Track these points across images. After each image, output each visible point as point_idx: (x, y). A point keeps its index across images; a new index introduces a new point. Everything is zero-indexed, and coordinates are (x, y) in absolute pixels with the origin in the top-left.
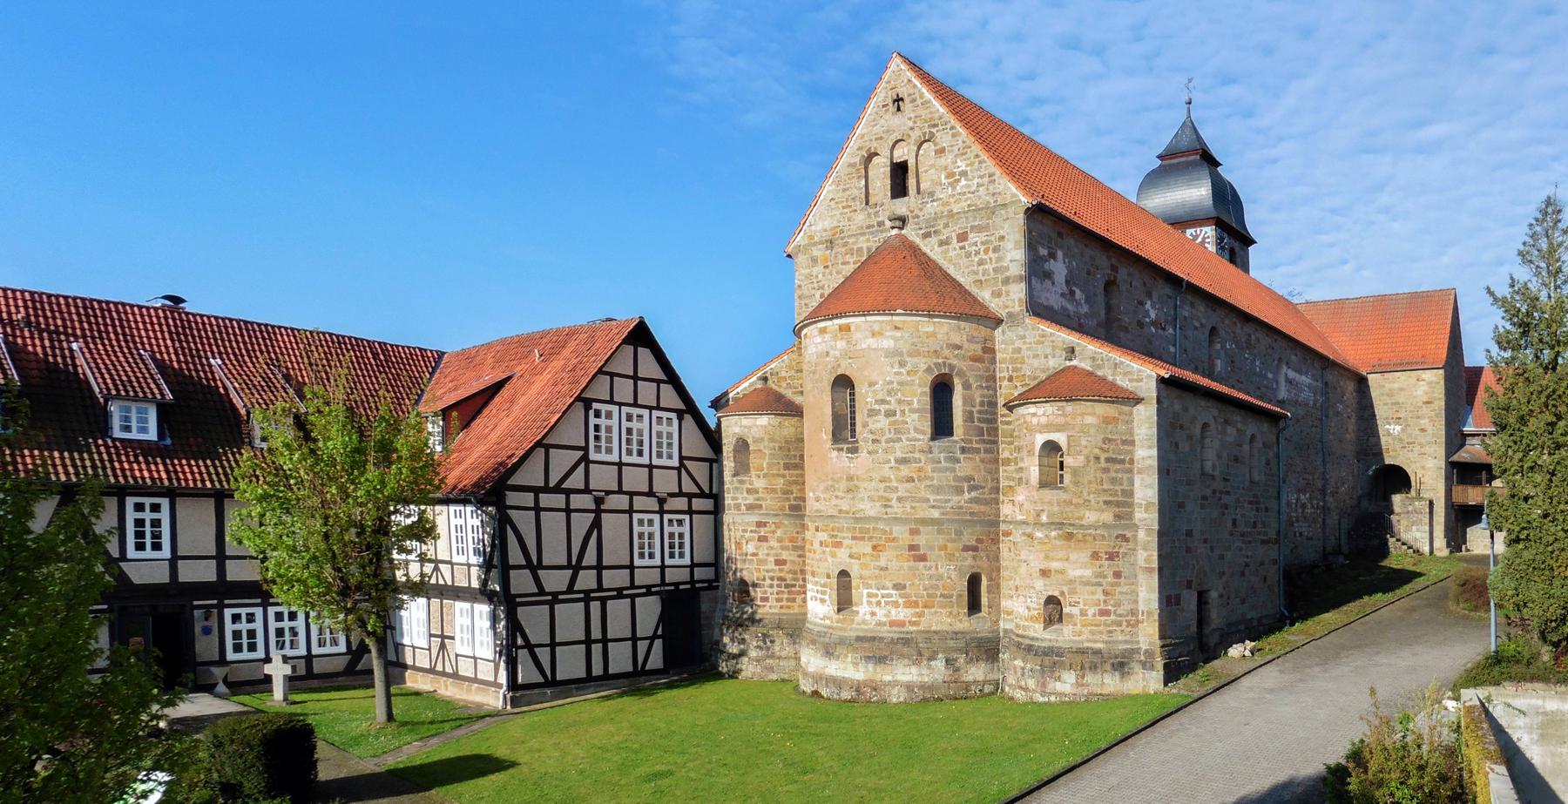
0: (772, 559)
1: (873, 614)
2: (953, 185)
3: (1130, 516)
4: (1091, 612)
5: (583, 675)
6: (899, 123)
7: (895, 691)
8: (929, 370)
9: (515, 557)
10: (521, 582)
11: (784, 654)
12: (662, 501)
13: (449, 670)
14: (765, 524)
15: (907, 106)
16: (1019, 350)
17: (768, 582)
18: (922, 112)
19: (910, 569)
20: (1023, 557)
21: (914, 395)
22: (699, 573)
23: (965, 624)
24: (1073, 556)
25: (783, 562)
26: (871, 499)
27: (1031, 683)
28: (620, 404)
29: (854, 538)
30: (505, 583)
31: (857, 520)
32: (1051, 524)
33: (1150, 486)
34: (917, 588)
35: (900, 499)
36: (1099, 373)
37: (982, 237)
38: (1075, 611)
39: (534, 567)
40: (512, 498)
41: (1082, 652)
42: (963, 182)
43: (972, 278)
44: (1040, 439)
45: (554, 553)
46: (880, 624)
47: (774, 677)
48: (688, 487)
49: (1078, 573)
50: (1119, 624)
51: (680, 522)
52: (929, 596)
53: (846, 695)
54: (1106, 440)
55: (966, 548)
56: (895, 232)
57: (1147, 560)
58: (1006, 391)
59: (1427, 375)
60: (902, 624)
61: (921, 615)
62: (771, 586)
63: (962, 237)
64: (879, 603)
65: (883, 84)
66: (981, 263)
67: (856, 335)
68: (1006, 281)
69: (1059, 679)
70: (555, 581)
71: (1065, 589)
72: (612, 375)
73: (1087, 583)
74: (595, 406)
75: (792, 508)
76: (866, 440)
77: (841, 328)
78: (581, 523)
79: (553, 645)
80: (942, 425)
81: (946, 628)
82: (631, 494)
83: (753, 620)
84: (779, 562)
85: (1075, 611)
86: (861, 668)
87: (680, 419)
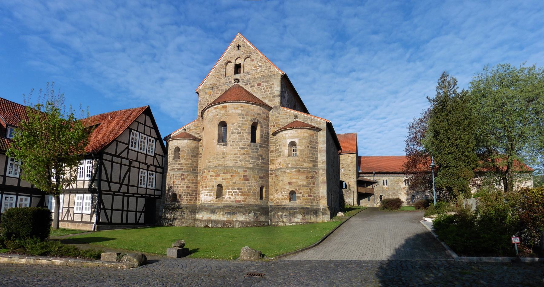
0: (185, 186)
1: (230, 198)
2: (256, 70)
3: (316, 166)
4: (305, 196)
5: (120, 222)
6: (238, 53)
7: (237, 224)
8: (251, 120)
9: (104, 177)
10: (104, 186)
11: (188, 218)
12: (148, 166)
13: (70, 219)
14: (184, 175)
15: (241, 48)
16: (278, 117)
17: (184, 194)
18: (247, 50)
19: (244, 183)
20: (281, 179)
21: (246, 128)
22: (157, 193)
23: (259, 202)
24: (300, 177)
25: (189, 187)
26: (231, 160)
27: (285, 220)
28: (140, 132)
29: (224, 173)
30: (99, 186)
31: (226, 167)
32: (292, 168)
33: (324, 156)
34: (245, 189)
35: (241, 160)
36: (306, 122)
37: (266, 84)
38: (301, 195)
39: (109, 181)
40: (105, 157)
41: (303, 208)
42: (260, 69)
43: (262, 96)
44: (289, 141)
45: (115, 178)
46: (232, 201)
47: (184, 225)
48: (156, 164)
49: (302, 183)
50: (314, 200)
51: (153, 175)
52: (249, 192)
53: (219, 226)
54: (311, 141)
55: (260, 178)
56: (236, 83)
57: (323, 179)
58: (272, 130)
59: (351, 155)
60: (239, 201)
61: (246, 199)
62: (185, 195)
63: (259, 85)
64: (232, 195)
65: (234, 42)
66: (265, 92)
67: (228, 109)
68: (274, 97)
69: (296, 217)
70: (115, 187)
71: (297, 188)
72: (139, 123)
73: (305, 186)
74: (133, 131)
75: (193, 170)
76: (230, 141)
77: (223, 107)
78: (125, 169)
79: (112, 210)
80: (253, 140)
81: (253, 203)
82: (140, 162)
83: (179, 208)
84: (187, 187)
85: (301, 195)
86: (225, 216)
87: (156, 141)
